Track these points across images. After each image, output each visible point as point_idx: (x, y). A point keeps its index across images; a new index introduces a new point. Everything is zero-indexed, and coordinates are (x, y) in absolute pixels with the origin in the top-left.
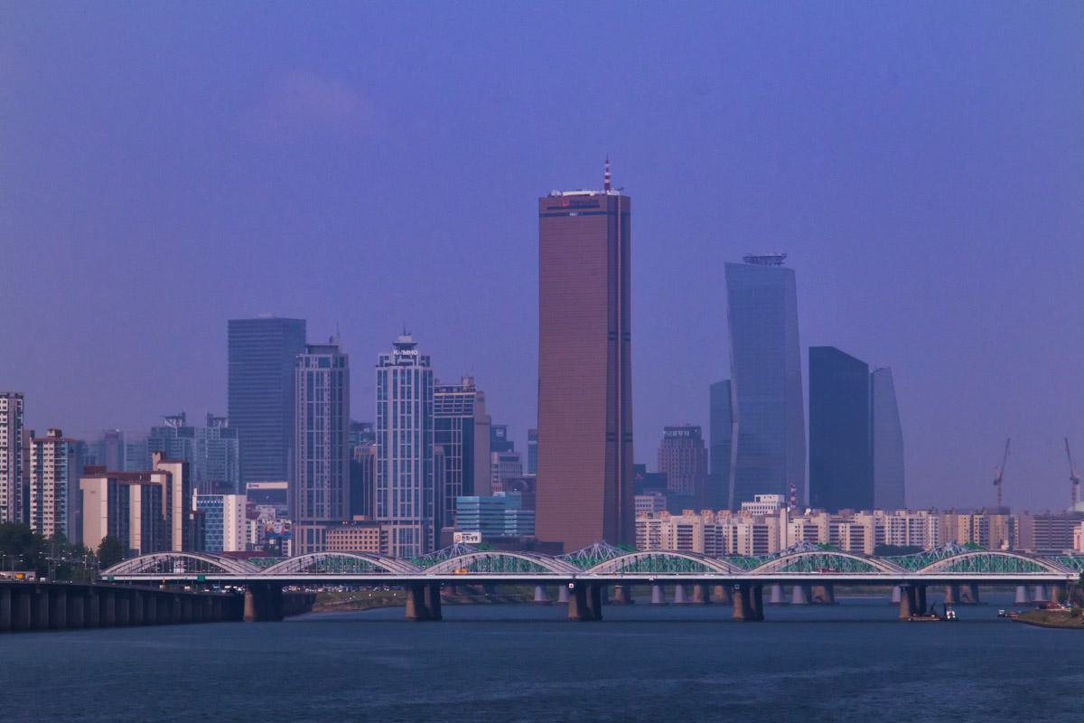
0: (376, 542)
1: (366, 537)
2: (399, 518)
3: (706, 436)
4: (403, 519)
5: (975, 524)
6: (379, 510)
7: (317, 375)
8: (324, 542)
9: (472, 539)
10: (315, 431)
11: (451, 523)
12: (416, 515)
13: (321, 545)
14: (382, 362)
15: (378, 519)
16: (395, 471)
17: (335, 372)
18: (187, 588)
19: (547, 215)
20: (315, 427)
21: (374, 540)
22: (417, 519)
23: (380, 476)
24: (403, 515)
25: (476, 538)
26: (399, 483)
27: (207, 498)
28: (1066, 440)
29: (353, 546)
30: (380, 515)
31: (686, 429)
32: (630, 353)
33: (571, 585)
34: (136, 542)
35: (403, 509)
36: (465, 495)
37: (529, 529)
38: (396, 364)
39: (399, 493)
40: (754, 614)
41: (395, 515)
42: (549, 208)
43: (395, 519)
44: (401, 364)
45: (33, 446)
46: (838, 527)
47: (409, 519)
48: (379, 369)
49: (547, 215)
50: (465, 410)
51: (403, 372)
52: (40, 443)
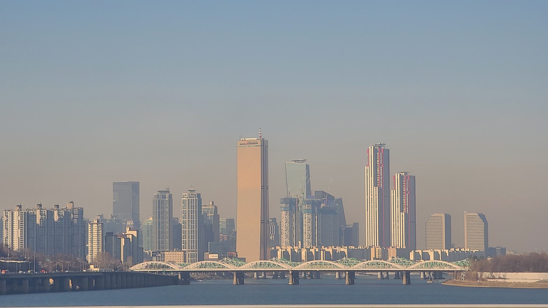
0: (182, 260)
1: (175, 258)
2: (190, 250)
4: (192, 250)
5: (376, 251)
6: (183, 247)
7: (162, 201)
8: (164, 258)
9: (215, 256)
10: (161, 220)
13: (163, 259)
14: (184, 196)
15: (183, 250)
16: (189, 234)
24: (191, 249)
25: (217, 256)
26: (190, 238)
27: (342, 254)
29: (170, 259)
30: (183, 249)
32: (523, 284)
34: (303, 258)
35: (191, 247)
38: (189, 197)
39: (190, 241)
40: (352, 282)
41: (189, 249)
42: (240, 144)
44: (191, 197)
45: (89, 225)
47: (194, 250)
48: (183, 199)
50: (211, 213)
51: (191, 199)
52: (92, 224)
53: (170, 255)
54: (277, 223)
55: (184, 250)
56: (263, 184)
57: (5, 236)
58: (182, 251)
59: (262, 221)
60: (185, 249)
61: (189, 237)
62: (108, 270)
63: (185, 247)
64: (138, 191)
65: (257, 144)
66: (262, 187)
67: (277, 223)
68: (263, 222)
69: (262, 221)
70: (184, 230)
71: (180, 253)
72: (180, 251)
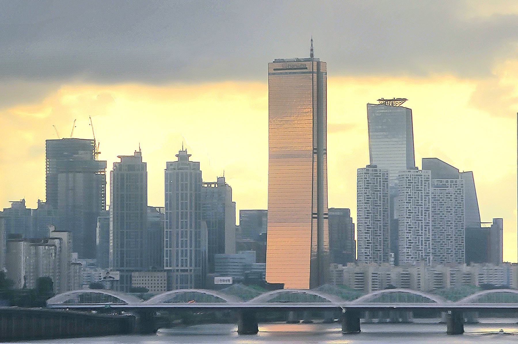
1: (161, 284)
2: (180, 268)
3: (354, 215)
4: (183, 268)
6: (167, 263)
11: (212, 271)
12: (191, 266)
15: (165, 268)
17: (424, 215)
18: (94, 312)
19: (274, 74)
20: (125, 209)
21: (163, 282)
22: (191, 268)
23: (167, 260)
24: (182, 266)
28: (76, 120)
31: (47, 169)
33: (450, 312)
35: (182, 263)
36: (220, 253)
37: (375, 282)
42: (274, 70)
43: (177, 268)
46: (199, 266)
47: (186, 268)
49: (274, 74)
53: (150, 279)
54: (4, 209)
55: (167, 268)
56: (316, 145)
57: (104, 306)
58: (165, 271)
59: (315, 149)
60: (170, 266)
61: (177, 244)
62: (144, 342)
63: (170, 263)
64: (48, 163)
65: (307, 68)
66: (315, 151)
67: (4, 209)
68: (316, 216)
69: (315, 149)
70: (169, 230)
71: (160, 274)
72: (162, 271)
